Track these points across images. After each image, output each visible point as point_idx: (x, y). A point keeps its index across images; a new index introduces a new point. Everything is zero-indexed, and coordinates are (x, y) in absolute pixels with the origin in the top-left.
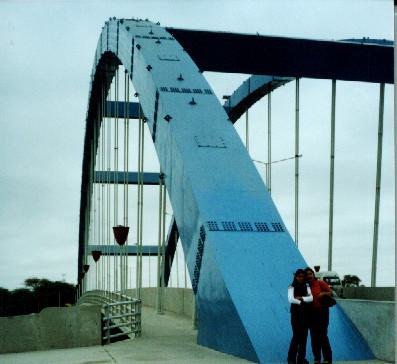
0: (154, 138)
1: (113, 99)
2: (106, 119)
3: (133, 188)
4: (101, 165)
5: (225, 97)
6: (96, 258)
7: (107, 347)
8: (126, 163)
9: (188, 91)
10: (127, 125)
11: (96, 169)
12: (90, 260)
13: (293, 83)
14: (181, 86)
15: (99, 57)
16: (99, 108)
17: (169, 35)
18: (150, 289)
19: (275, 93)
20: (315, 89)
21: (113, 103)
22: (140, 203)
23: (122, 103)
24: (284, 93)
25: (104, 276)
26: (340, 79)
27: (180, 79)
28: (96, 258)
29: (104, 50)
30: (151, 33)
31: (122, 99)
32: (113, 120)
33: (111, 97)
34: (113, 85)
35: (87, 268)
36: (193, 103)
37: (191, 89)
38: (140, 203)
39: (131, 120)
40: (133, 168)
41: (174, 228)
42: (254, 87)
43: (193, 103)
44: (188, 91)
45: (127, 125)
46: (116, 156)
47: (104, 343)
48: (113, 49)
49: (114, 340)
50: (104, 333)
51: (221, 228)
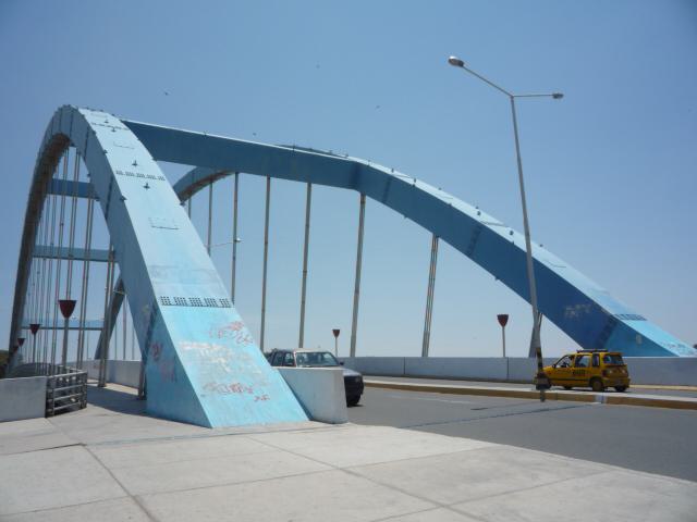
0: (106, 217)
1: (61, 177)
4: (42, 239)
6: (34, 332)
8: (53, 358)
9: (143, 176)
10: (75, 203)
11: (38, 243)
12: (26, 334)
14: (135, 170)
16: (44, 183)
17: (124, 126)
19: (217, 184)
20: (252, 183)
23: (68, 195)
24: (224, 185)
28: (34, 332)
29: (56, 131)
30: (35, 328)
31: (71, 178)
32: (59, 197)
33: (59, 175)
34: (62, 160)
35: (22, 341)
36: (147, 187)
37: (145, 174)
38: (86, 278)
39: (79, 199)
41: (121, 286)
42: (198, 178)
43: (147, 187)
44: (143, 176)
45: (75, 203)
46: (43, 295)
47: (47, 415)
48: (65, 131)
50: (48, 405)
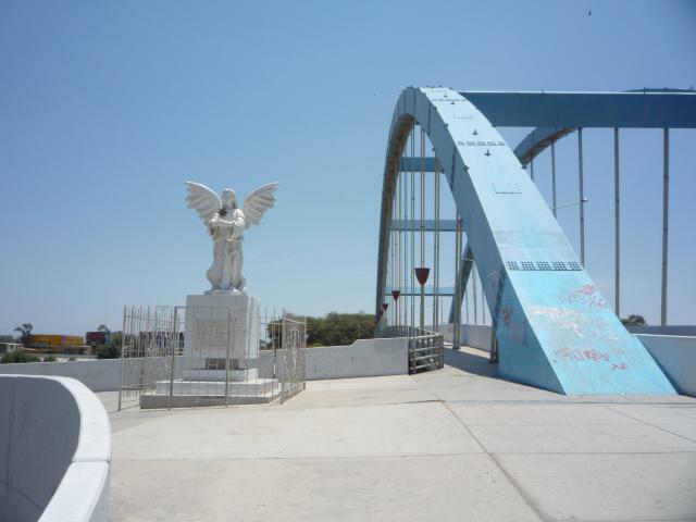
1: (409, 155)
2: (403, 174)
3: (429, 236)
5: (19, 329)
7: (413, 376)
8: (413, 322)
9: (483, 144)
10: (423, 177)
12: (389, 300)
13: (574, 135)
14: (475, 139)
15: (396, 120)
16: (396, 163)
18: (430, 221)
20: (597, 138)
21: (409, 159)
22: (437, 247)
24: (566, 144)
25: (403, 313)
26: (625, 126)
27: (475, 134)
29: (402, 112)
30: (396, 295)
32: (409, 174)
34: (409, 143)
35: (386, 306)
36: (488, 154)
37: (486, 142)
38: (437, 247)
40: (430, 216)
41: (469, 253)
43: (488, 154)
44: (483, 144)
45: (423, 177)
47: (410, 373)
48: (411, 113)
49: (419, 371)
51: (537, 268)
